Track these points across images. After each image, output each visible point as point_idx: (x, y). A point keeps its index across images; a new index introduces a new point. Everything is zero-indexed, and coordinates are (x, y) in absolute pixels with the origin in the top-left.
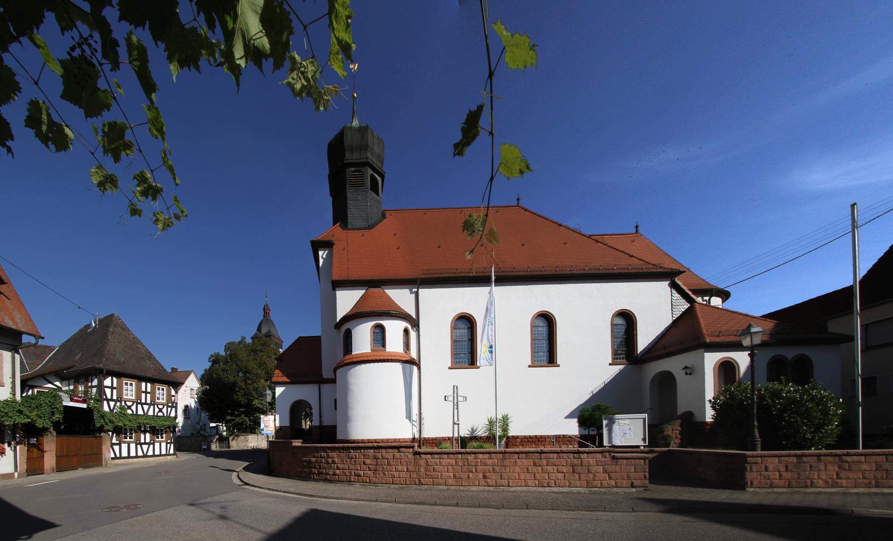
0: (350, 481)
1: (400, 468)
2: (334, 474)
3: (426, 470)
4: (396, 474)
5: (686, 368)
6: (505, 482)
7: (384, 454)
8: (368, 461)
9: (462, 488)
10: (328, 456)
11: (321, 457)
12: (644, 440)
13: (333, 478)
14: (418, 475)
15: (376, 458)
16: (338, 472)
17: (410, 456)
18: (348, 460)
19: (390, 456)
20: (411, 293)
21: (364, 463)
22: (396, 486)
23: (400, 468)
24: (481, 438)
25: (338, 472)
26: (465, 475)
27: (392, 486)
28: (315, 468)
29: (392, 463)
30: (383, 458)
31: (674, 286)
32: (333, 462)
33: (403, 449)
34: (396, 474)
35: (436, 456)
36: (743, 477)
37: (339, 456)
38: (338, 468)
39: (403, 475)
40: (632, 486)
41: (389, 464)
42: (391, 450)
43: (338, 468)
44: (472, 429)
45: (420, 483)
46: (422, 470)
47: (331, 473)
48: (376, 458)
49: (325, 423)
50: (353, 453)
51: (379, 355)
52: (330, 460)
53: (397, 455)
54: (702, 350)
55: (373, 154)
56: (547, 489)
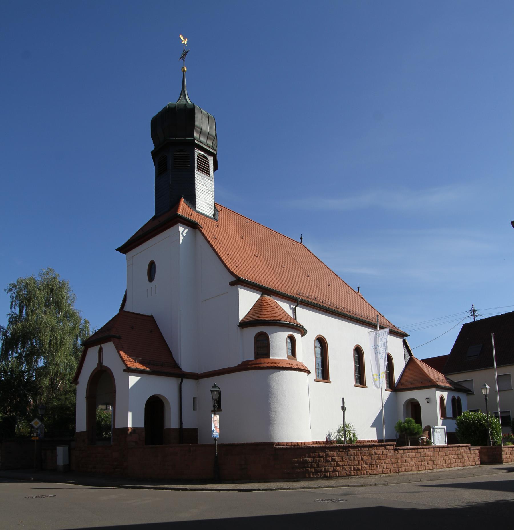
0: (350, 475)
1: (387, 461)
2: (335, 471)
3: (402, 462)
4: (385, 466)
5: (427, 398)
6: (435, 466)
7: (376, 451)
8: (365, 457)
9: (419, 472)
10: (327, 455)
11: (319, 456)
12: (445, 441)
13: (333, 474)
14: (397, 465)
15: (370, 454)
16: (338, 468)
17: (392, 451)
18: (348, 458)
19: (380, 452)
20: (291, 308)
21: (362, 459)
22: (384, 475)
23: (387, 461)
24: (334, 442)
25: (338, 468)
26: (419, 463)
27: (382, 475)
28: (312, 467)
29: (382, 458)
30: (375, 454)
31: (405, 343)
32: (334, 460)
33: (388, 447)
34: (385, 466)
35: (406, 451)
36: (501, 458)
37: (338, 455)
38: (338, 465)
39: (389, 466)
40: (476, 465)
41: (380, 459)
42: (380, 448)
43: (338, 465)
44: (329, 435)
45: (399, 471)
46: (399, 461)
47: (331, 470)
48: (370, 454)
49: (184, 426)
50: (351, 452)
51: (292, 363)
52: (330, 459)
53: (385, 451)
54: (435, 389)
55: (201, 133)
56: (450, 469)
